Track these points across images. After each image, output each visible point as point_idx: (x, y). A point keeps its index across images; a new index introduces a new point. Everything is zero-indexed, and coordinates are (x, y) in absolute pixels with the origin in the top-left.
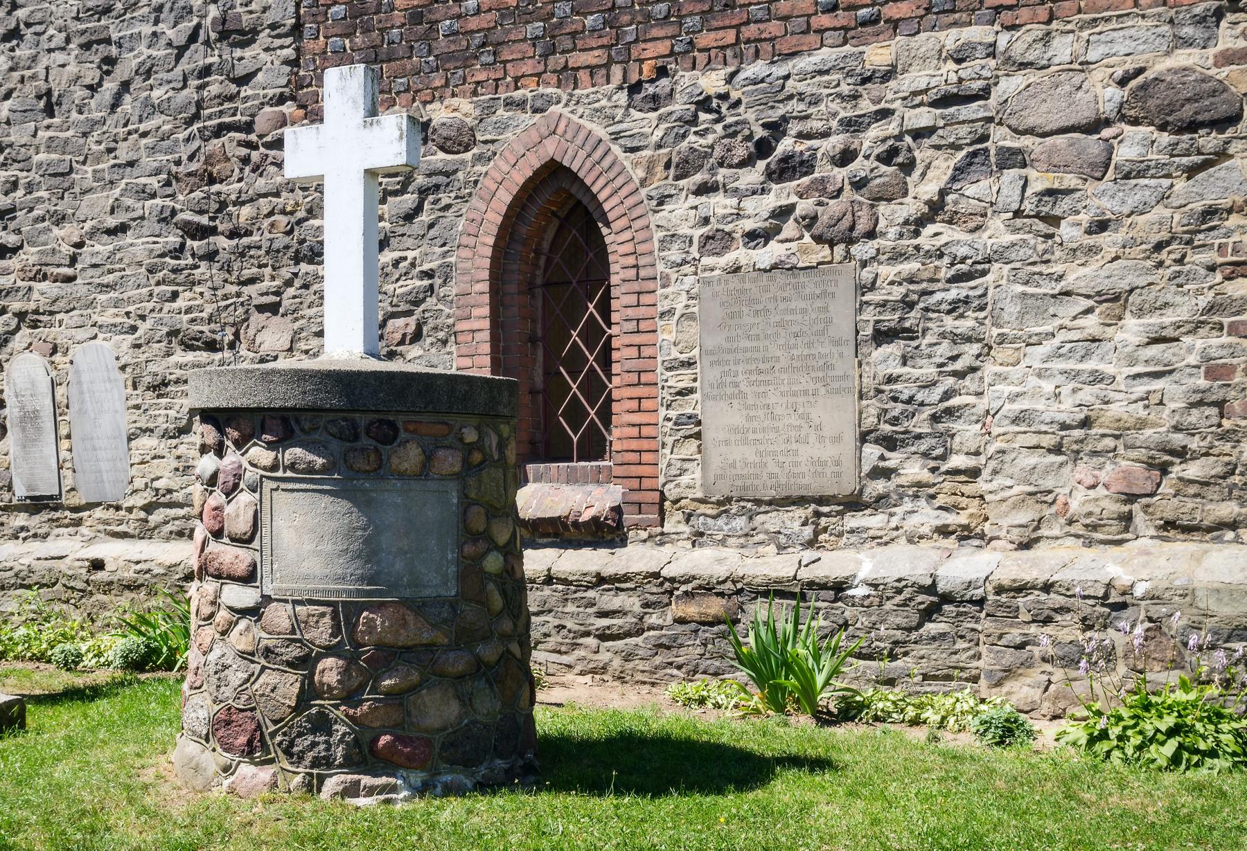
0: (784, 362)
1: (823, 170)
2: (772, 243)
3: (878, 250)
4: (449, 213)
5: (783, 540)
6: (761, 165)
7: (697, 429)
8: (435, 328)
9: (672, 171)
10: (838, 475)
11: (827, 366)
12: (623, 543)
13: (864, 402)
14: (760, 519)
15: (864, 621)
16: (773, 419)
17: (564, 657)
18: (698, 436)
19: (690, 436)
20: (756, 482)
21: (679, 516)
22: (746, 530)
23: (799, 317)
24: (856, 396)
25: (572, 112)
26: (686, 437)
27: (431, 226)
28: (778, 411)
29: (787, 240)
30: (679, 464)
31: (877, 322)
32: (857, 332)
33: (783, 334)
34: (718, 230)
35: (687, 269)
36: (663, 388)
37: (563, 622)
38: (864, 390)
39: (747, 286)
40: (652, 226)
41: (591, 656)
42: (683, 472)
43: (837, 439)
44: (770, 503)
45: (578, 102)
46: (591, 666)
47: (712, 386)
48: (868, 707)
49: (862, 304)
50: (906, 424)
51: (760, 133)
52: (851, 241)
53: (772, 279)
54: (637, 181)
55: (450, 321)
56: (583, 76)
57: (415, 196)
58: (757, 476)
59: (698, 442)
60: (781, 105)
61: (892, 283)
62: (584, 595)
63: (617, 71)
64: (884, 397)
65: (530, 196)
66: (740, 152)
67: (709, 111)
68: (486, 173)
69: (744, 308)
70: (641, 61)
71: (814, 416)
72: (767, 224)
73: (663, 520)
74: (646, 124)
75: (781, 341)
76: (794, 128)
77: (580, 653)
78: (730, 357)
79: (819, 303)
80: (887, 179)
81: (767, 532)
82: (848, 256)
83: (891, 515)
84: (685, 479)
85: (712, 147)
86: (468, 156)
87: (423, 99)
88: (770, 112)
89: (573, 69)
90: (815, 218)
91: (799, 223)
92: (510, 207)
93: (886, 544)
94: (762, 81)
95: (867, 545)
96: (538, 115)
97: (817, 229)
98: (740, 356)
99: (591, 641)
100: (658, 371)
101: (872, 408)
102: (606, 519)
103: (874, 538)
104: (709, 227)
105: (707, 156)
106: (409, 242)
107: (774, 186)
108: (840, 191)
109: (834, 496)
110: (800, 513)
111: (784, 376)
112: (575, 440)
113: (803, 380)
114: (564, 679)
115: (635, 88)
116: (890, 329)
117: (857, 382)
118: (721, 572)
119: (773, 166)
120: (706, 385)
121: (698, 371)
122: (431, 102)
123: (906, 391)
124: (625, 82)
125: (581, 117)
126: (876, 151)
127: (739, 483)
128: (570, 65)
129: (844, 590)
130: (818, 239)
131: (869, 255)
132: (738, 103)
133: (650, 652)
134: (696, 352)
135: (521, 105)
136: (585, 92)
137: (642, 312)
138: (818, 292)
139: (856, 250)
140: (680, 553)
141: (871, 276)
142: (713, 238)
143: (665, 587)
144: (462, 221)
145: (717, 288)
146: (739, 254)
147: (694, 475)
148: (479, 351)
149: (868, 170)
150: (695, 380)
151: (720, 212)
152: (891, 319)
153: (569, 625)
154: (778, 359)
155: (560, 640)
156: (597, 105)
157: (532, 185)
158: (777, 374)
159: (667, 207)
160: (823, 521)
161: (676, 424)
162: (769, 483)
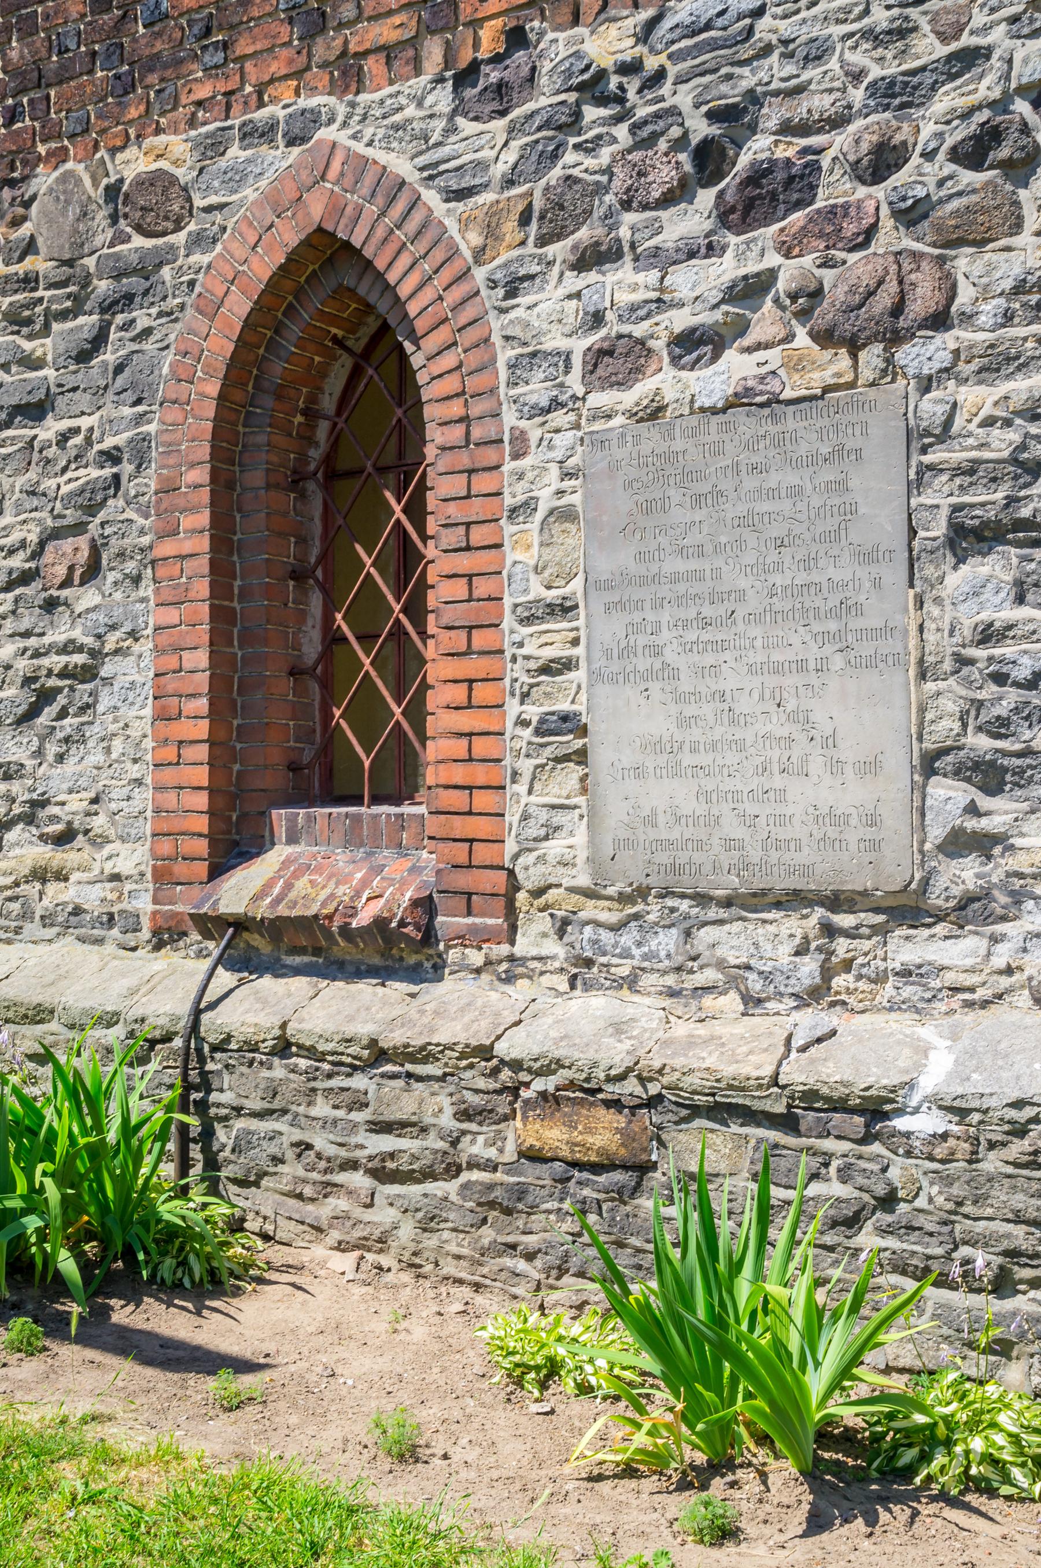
0: (754, 603)
1: (836, 188)
2: (731, 356)
3: (956, 353)
4: (149, 346)
5: (755, 984)
6: (706, 198)
7: (579, 743)
8: (121, 555)
9: (533, 227)
10: (875, 845)
11: (847, 608)
12: (437, 971)
13: (930, 686)
14: (706, 935)
15: (933, 1196)
16: (732, 722)
17: (310, 1207)
18: (581, 757)
19: (566, 758)
20: (698, 857)
21: (543, 923)
22: (679, 959)
23: (786, 505)
24: (912, 673)
25: (354, 137)
26: (558, 760)
27: (119, 369)
28: (744, 705)
29: (759, 346)
30: (544, 815)
31: (957, 508)
32: (913, 532)
33: (752, 542)
34: (620, 337)
35: (560, 418)
36: (514, 659)
37: (306, 1137)
38: (930, 659)
39: (678, 445)
40: (496, 339)
41: (358, 1212)
42: (551, 831)
43: (871, 767)
44: (728, 903)
45: (365, 117)
46: (357, 1233)
47: (608, 654)
48: (948, 1444)
49: (925, 469)
50: (1027, 735)
51: (701, 129)
52: (895, 338)
53: (726, 428)
54: (468, 254)
55: (145, 540)
56: (373, 66)
57: (95, 317)
58: (700, 845)
59: (580, 770)
60: (746, 71)
61: (989, 422)
62: (346, 1083)
63: (434, 52)
64: (974, 673)
65: (290, 306)
66: (663, 175)
67: (602, 101)
68: (209, 266)
69: (671, 492)
70: (476, 24)
71: (818, 716)
72: (718, 316)
73: (513, 928)
74: (489, 143)
75: (749, 558)
76: (772, 116)
77: (339, 1203)
78: (644, 594)
79: (828, 474)
80: (974, 198)
81: (721, 965)
82: (890, 369)
83: (995, 939)
84: (554, 848)
85: (608, 171)
86: (180, 238)
87: (111, 144)
88: (724, 88)
89: (356, 55)
90: (817, 294)
91: (783, 308)
92: (248, 324)
93: (985, 1004)
94: (708, 27)
95: (942, 1007)
96: (296, 151)
97: (825, 314)
98: (664, 591)
99: (359, 1180)
100: (505, 625)
101: (949, 697)
102: (402, 924)
103: (955, 990)
104: (603, 332)
105: (601, 189)
106: (83, 400)
107: (733, 239)
108: (870, 232)
109: (865, 893)
110: (793, 926)
111: (756, 631)
112: (367, 764)
113: (796, 640)
114: (305, 1257)
115: (467, 76)
116: (985, 524)
117: (913, 642)
118: (616, 1054)
119: (730, 198)
120: (597, 654)
121: (581, 623)
122: (123, 148)
123: (1025, 660)
124: (446, 68)
125: (370, 144)
126: (949, 142)
127: (663, 858)
128: (353, 48)
129: (886, 1116)
130: (824, 338)
131: (937, 365)
132: (660, 75)
133: (470, 1218)
134: (576, 585)
135: (266, 133)
136: (377, 96)
137: (476, 509)
138: (825, 450)
139: (907, 355)
140: (545, 1001)
141: (941, 409)
142: (610, 353)
143: (501, 1083)
144: (170, 357)
145: (619, 453)
146: (664, 381)
147: (573, 840)
148: (192, 595)
149: (931, 181)
150: (575, 642)
151: (625, 298)
152: (988, 499)
153: (321, 1142)
154: (741, 596)
155: (301, 1172)
156: (397, 118)
157: (288, 285)
158: (741, 627)
159: (523, 300)
160: (842, 946)
161: (538, 732)
162: (725, 862)
